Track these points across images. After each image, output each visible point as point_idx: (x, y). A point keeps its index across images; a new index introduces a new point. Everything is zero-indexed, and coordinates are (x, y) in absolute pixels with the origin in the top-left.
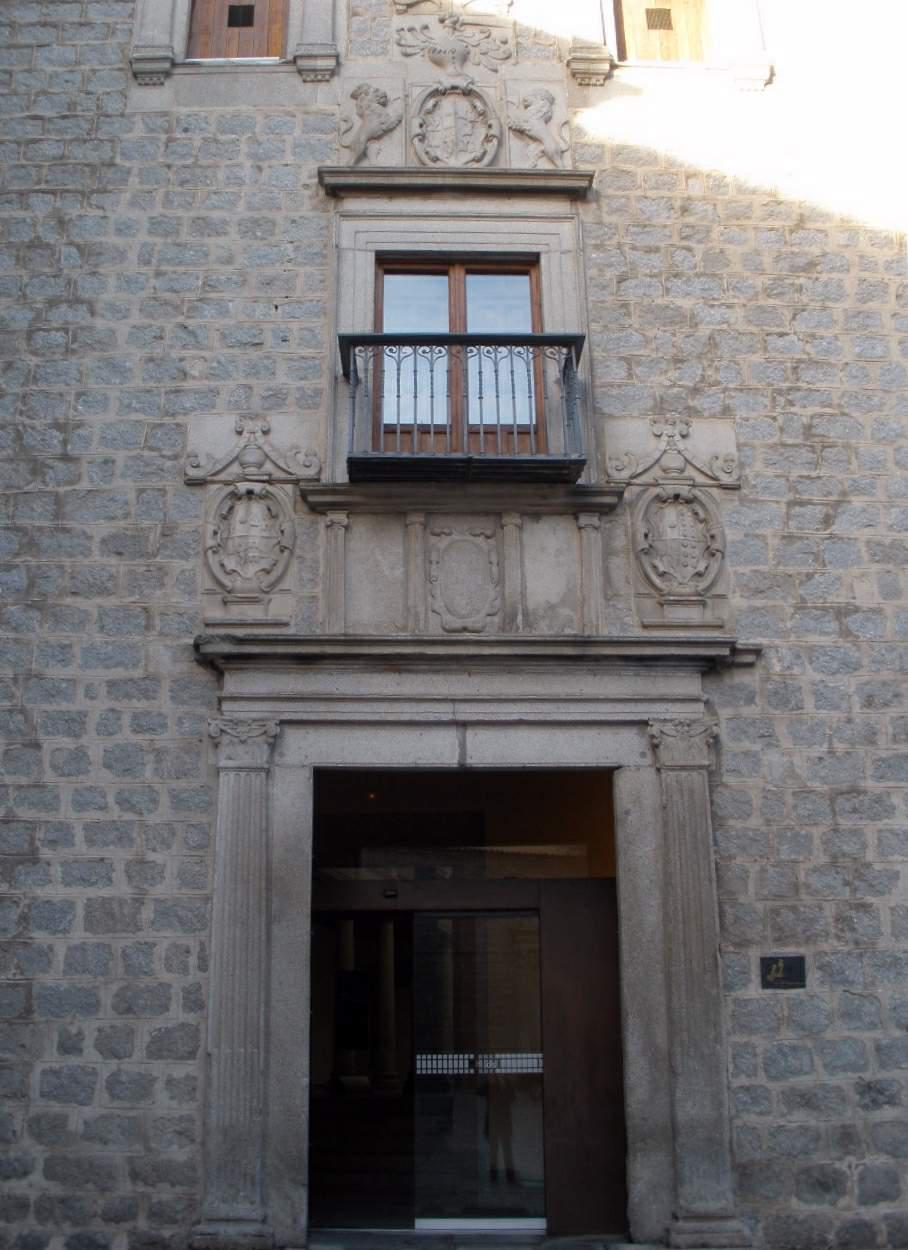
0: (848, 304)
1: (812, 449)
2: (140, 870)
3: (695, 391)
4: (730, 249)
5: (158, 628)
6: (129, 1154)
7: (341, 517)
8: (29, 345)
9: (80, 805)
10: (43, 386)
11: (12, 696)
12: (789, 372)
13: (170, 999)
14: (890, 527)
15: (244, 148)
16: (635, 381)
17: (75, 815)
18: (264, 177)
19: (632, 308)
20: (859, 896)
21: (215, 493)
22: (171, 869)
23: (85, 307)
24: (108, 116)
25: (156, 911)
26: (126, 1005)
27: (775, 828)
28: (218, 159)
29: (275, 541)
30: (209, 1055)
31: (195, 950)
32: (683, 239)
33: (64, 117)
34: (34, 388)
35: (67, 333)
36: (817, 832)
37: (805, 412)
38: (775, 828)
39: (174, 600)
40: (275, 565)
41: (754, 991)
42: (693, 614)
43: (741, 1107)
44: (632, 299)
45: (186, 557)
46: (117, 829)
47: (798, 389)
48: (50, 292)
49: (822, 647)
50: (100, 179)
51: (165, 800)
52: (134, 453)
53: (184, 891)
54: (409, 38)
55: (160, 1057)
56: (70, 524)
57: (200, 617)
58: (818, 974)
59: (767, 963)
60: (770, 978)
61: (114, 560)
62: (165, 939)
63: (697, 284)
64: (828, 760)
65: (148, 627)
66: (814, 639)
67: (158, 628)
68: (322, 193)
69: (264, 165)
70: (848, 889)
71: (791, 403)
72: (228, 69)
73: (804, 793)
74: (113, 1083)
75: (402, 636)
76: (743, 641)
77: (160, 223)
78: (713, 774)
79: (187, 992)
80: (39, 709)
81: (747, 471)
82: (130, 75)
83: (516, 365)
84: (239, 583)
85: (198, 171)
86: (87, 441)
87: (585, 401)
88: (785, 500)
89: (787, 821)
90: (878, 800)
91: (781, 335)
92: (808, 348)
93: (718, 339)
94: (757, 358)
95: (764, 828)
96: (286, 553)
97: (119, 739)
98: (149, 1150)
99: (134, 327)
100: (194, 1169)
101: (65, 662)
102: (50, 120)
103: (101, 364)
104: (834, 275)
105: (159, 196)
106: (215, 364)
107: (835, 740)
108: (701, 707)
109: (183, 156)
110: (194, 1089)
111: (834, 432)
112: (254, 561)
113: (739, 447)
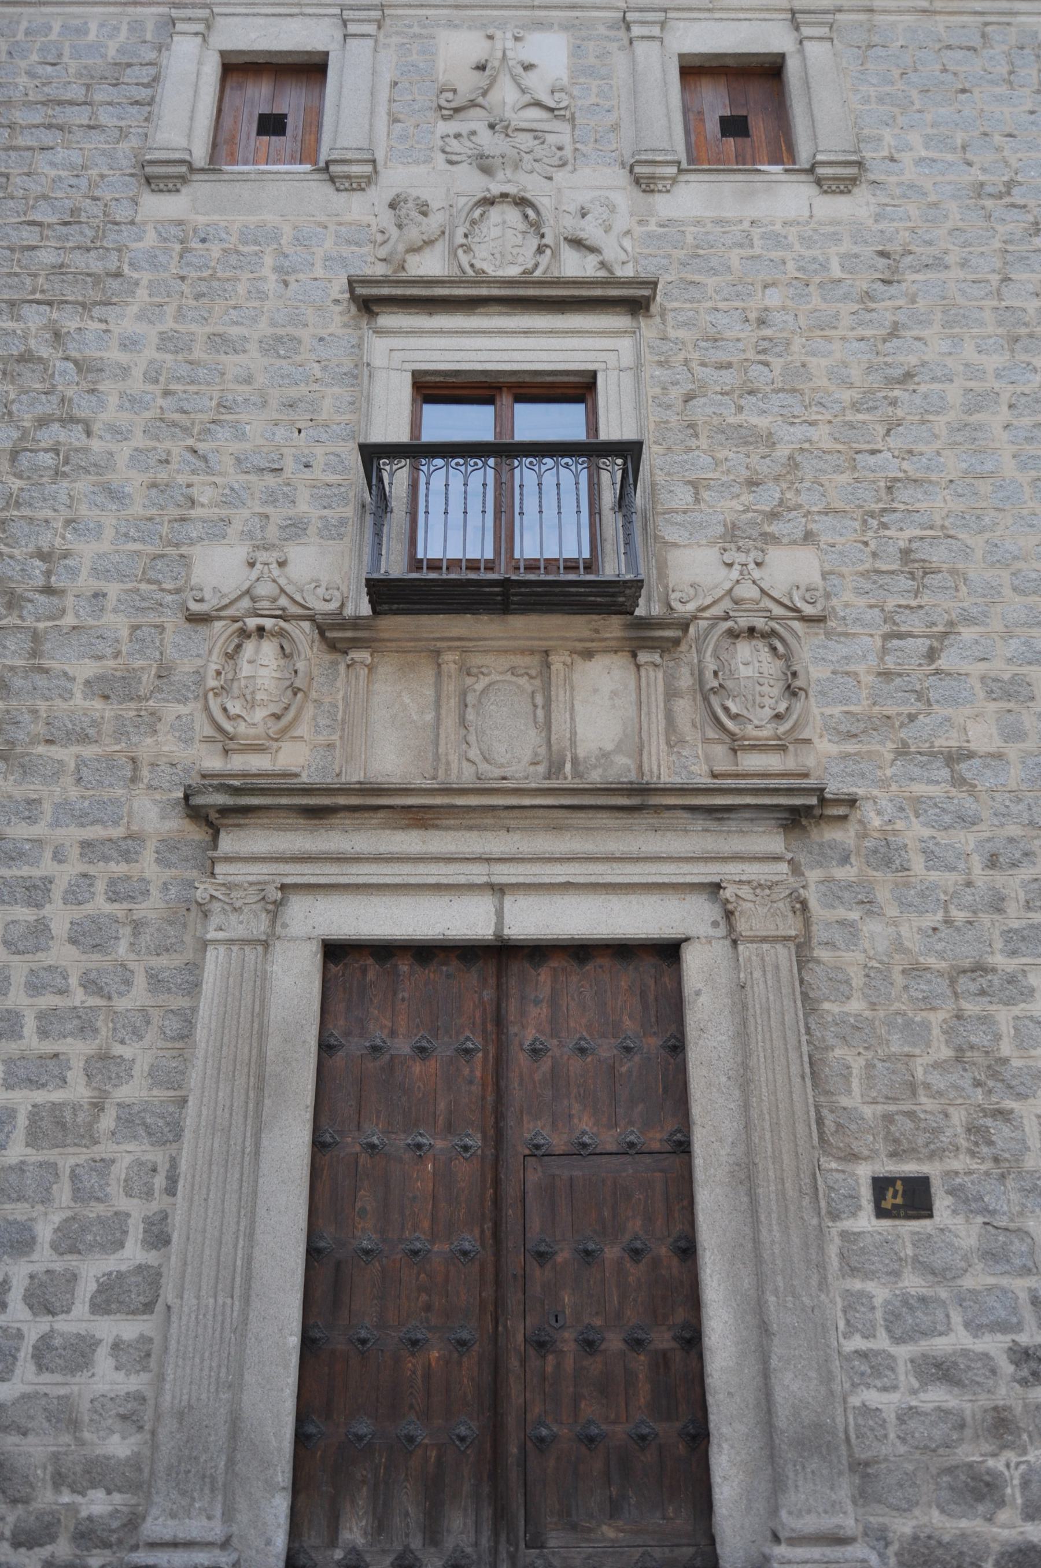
0: (951, 416)
1: (912, 576)
3: (773, 516)
4: (813, 362)
5: (146, 781)
6: (55, 1449)
8: (12, 466)
9: (34, 988)
10: (26, 512)
12: (883, 492)
13: (125, 1232)
15: (269, 260)
16: (703, 506)
17: (28, 1001)
18: (290, 293)
19: (699, 429)
20: (994, 1099)
22: (141, 1068)
24: (116, 224)
25: (119, 1118)
26: (71, 1240)
27: (882, 1014)
28: (238, 272)
29: (288, 683)
30: (169, 1308)
31: (163, 1169)
32: (759, 352)
33: (66, 224)
34: (16, 513)
35: (58, 455)
36: (936, 1019)
37: (902, 537)
38: (882, 1014)
39: (165, 748)
40: (286, 709)
41: (865, 1221)
42: (772, 762)
43: (857, 1380)
44: (700, 419)
45: (184, 700)
46: (79, 1017)
47: (895, 510)
48: (40, 410)
49: (930, 798)
50: (104, 291)
51: (140, 981)
52: (129, 586)
53: (155, 1092)
54: (454, 145)
55: (108, 1312)
56: (47, 663)
57: (197, 767)
58: (949, 1201)
59: (881, 1185)
60: (887, 1205)
61: (98, 704)
62: (128, 1154)
63: (776, 400)
64: (945, 932)
65: (134, 780)
66: (919, 789)
67: (146, 781)
68: (353, 309)
69: (291, 279)
70: (979, 1090)
71: (885, 526)
72: (253, 177)
73: (915, 971)
75: (428, 784)
76: (834, 788)
77: (170, 339)
79: (149, 1223)
81: (834, 601)
82: (143, 181)
83: (568, 478)
84: (242, 728)
85: (215, 284)
86: (74, 572)
87: (645, 528)
88: (880, 633)
89: (897, 1005)
90: (1012, 980)
91: (873, 452)
92: (905, 465)
93: (799, 459)
94: (844, 478)
95: (867, 1013)
96: (300, 695)
97: (89, 908)
98: (81, 1443)
99: (136, 450)
100: (140, 1470)
101: (32, 820)
102: (50, 226)
103: (96, 489)
104: (936, 386)
105: (170, 310)
106: (227, 491)
107: (952, 907)
108: (784, 867)
110: (148, 1355)
111: (937, 555)
112: (263, 704)
113: (824, 575)
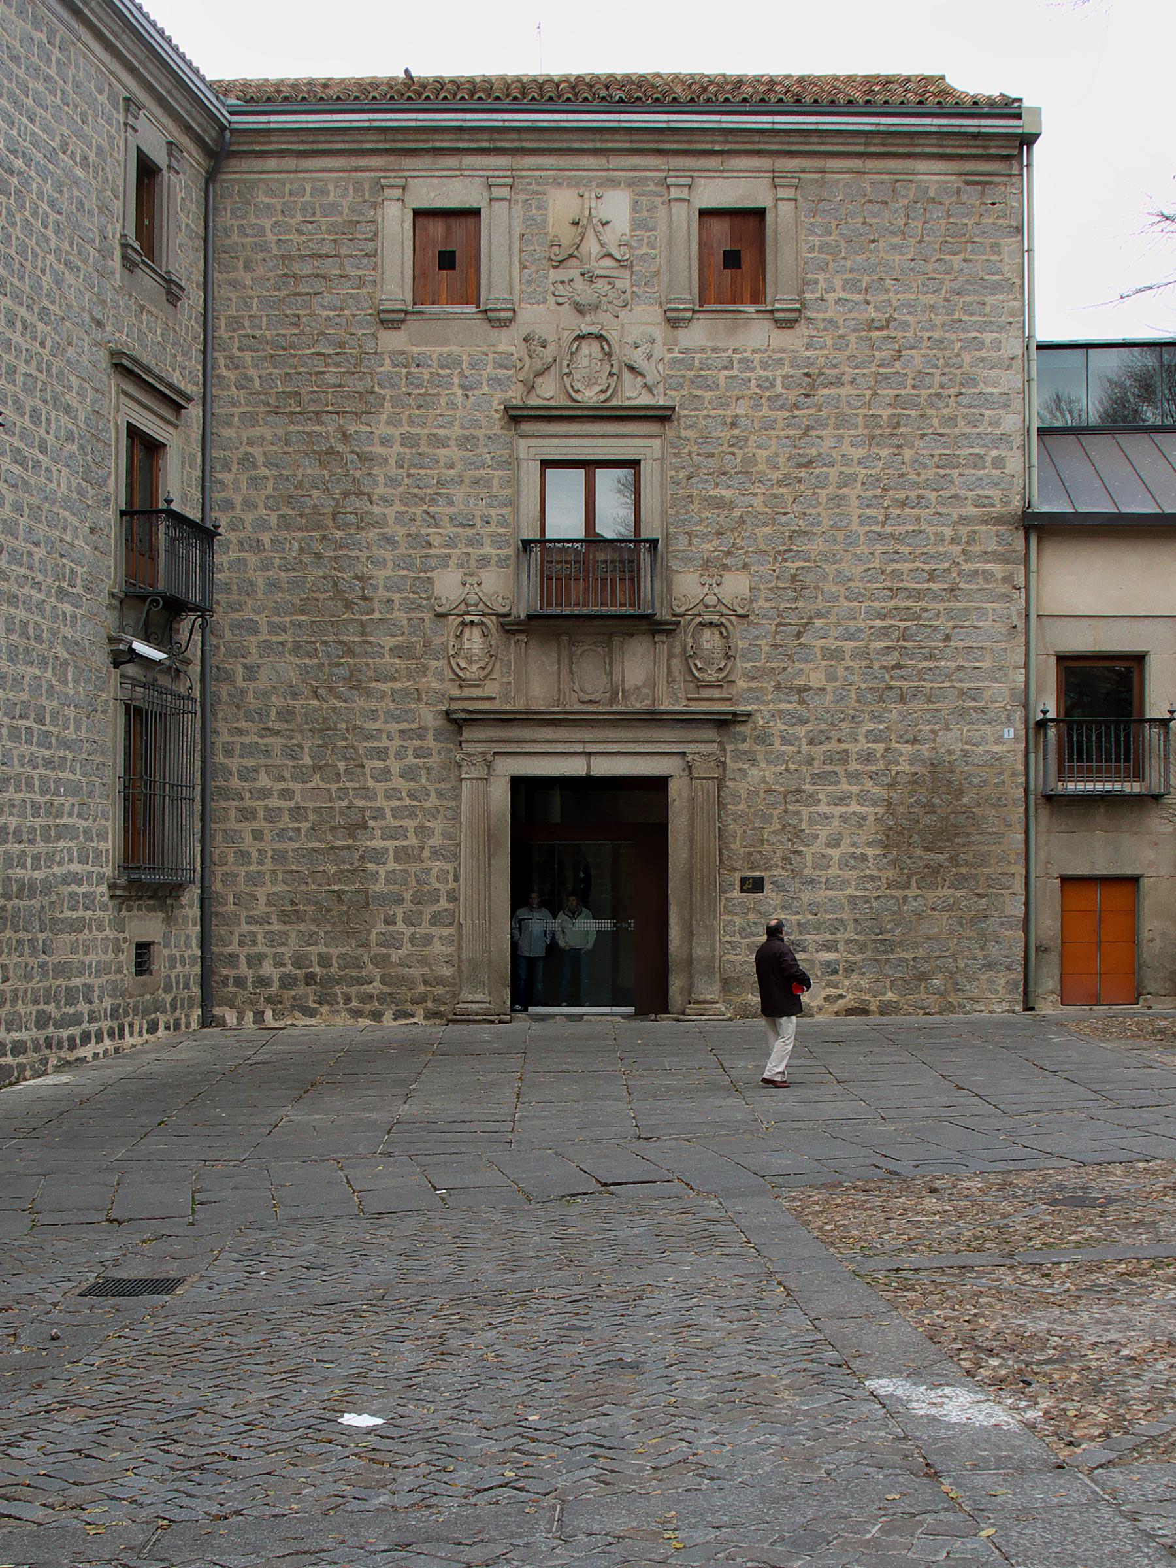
2: (421, 829)
3: (728, 553)
7: (523, 637)
9: (388, 798)
11: (346, 739)
14: (836, 639)
21: (454, 621)
23: (366, 498)
26: (417, 901)
31: (452, 871)
37: (792, 566)
41: (736, 894)
45: (438, 659)
50: (366, 403)
51: (433, 794)
56: (370, 639)
59: (743, 880)
61: (397, 661)
62: (437, 866)
65: (419, 700)
66: (783, 706)
69: (470, 393)
71: (785, 560)
72: (442, 316)
73: (769, 791)
74: (412, 939)
78: (721, 782)
80: (362, 746)
81: (754, 605)
85: (427, 398)
91: (785, 514)
94: (767, 530)
97: (407, 762)
98: (431, 970)
101: (375, 720)
104: (824, 469)
109: (417, 387)
111: (809, 579)
112: (476, 662)
113: (751, 589)
